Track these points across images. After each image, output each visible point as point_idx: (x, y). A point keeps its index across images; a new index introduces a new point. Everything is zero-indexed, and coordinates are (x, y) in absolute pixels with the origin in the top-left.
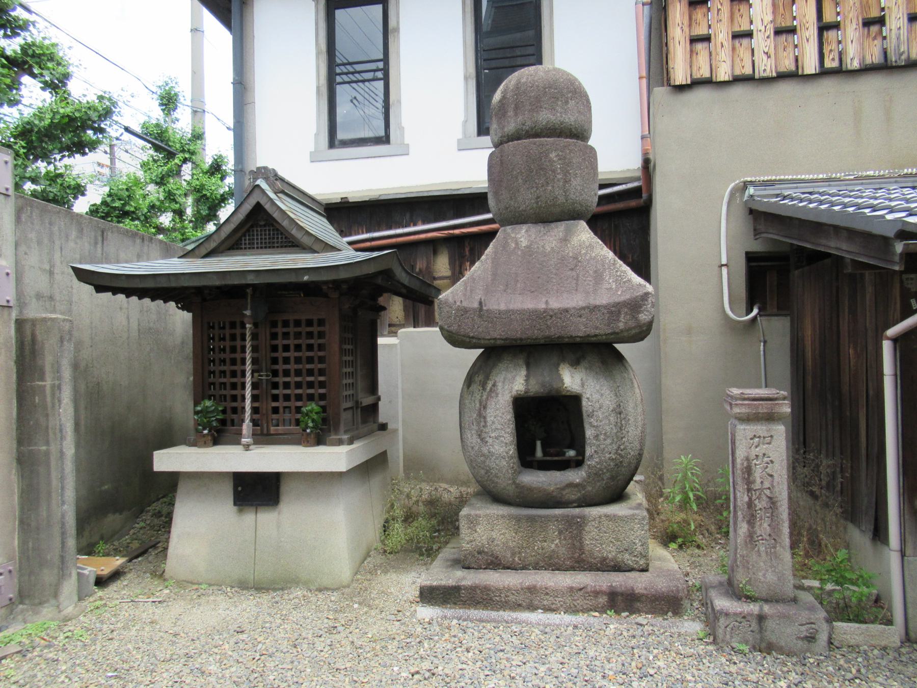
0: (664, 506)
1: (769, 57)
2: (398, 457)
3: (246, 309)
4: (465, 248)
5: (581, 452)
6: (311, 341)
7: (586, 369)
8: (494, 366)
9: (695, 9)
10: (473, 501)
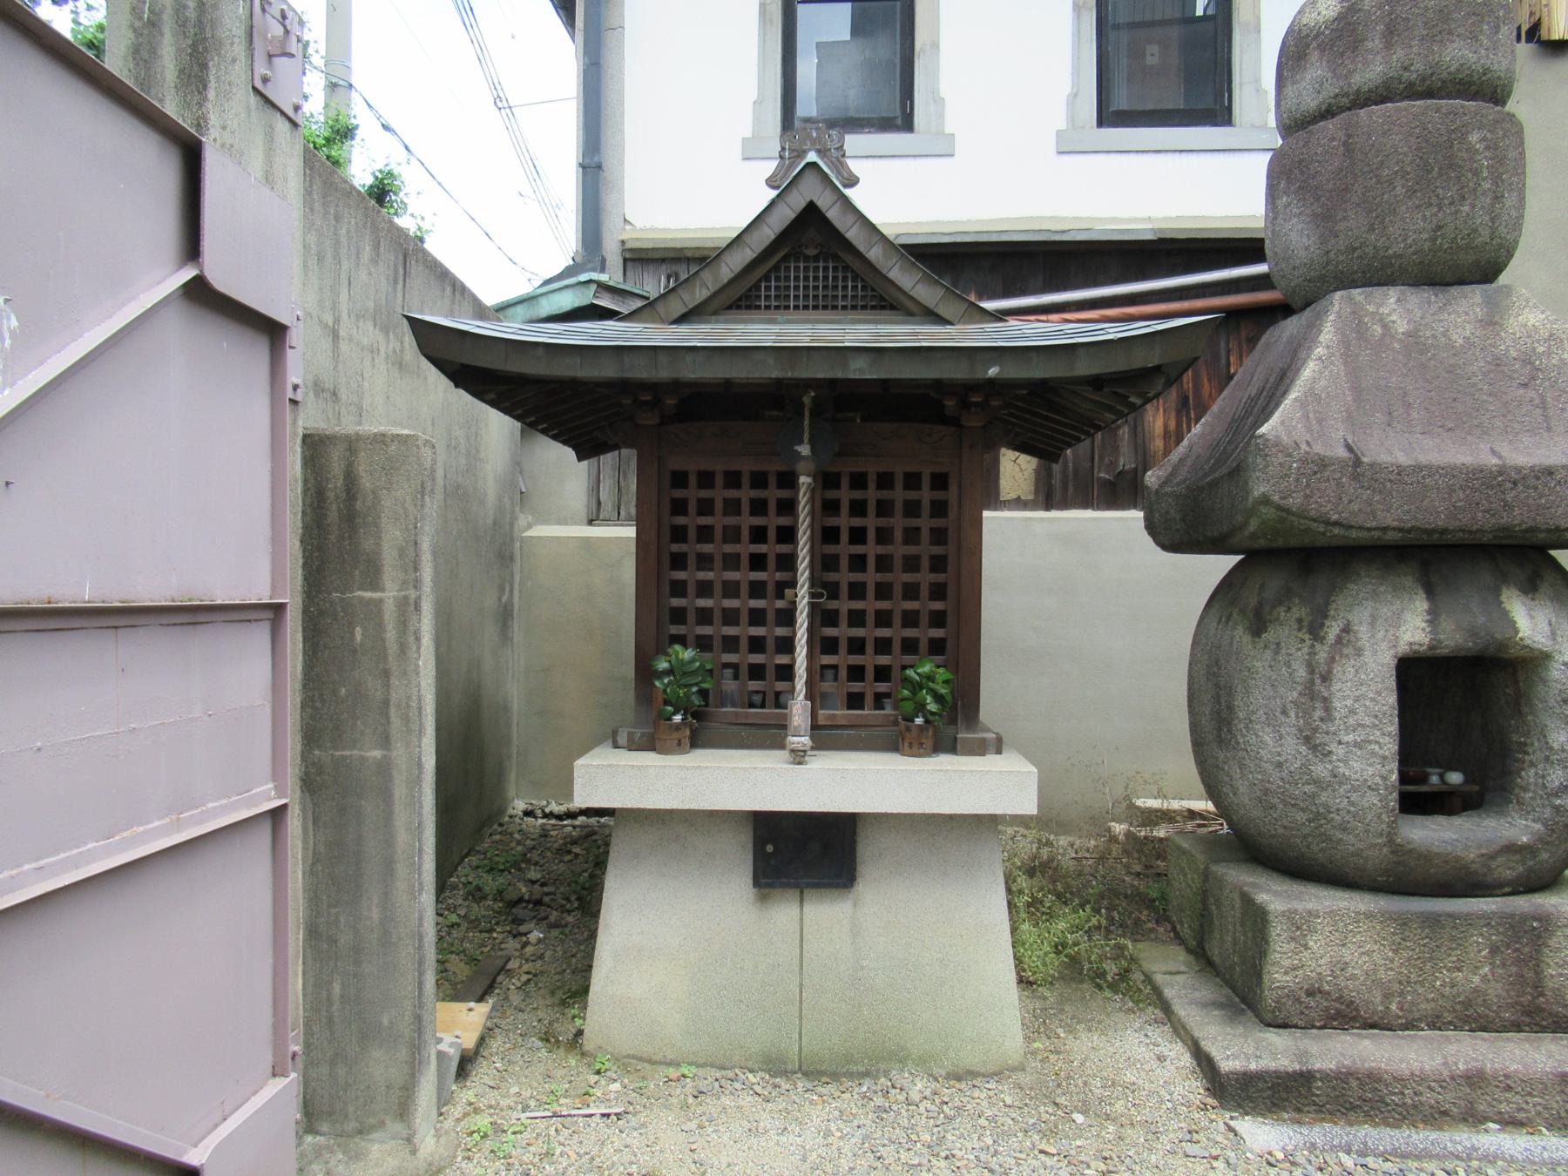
3: (801, 442)
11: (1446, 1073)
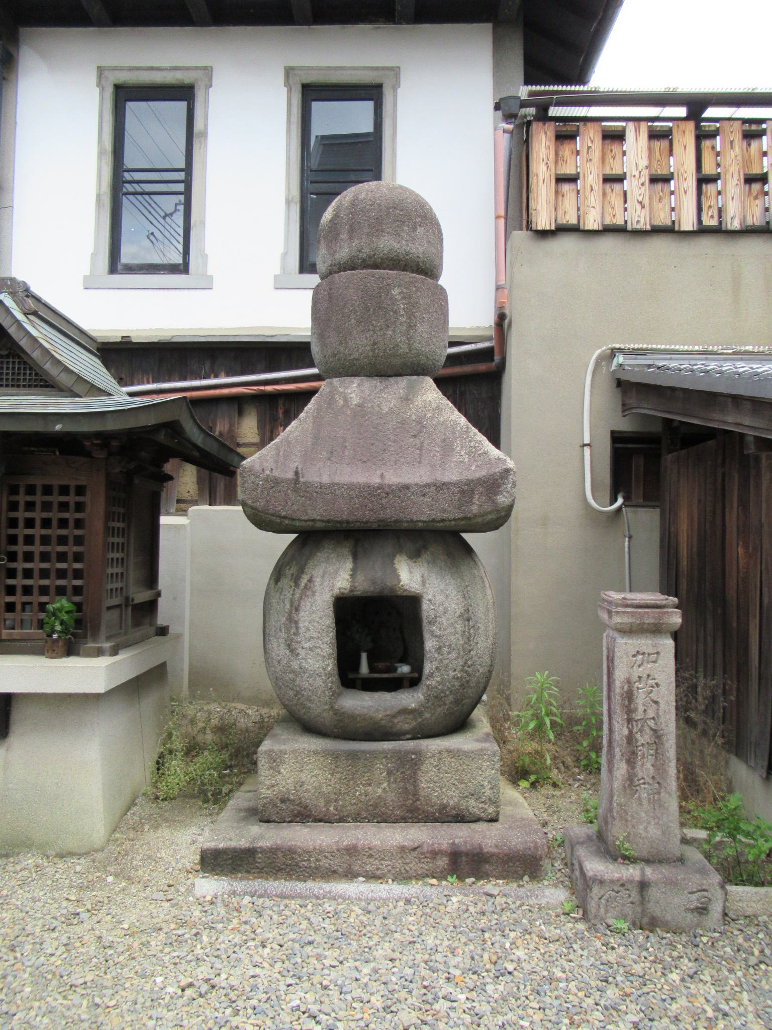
0: (514, 733)
1: (643, 207)
2: (182, 670)
4: (279, 408)
5: (418, 668)
6: (65, 515)
7: (428, 562)
8: (311, 556)
9: (562, 145)
10: (277, 730)
11: (335, 848)
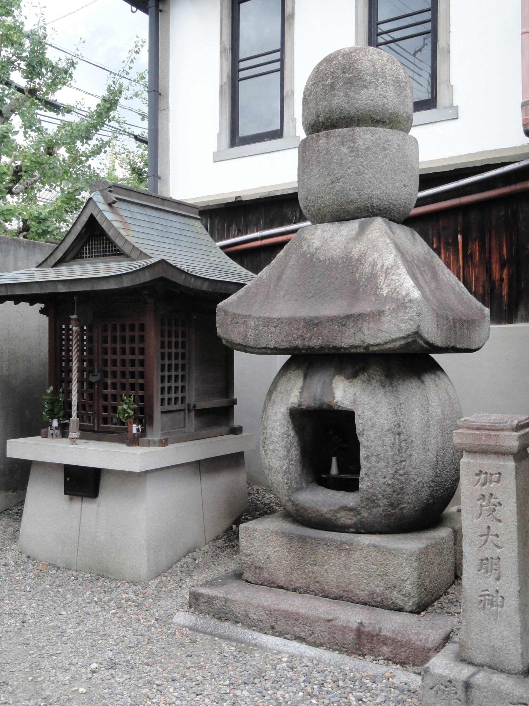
3: (73, 314)
